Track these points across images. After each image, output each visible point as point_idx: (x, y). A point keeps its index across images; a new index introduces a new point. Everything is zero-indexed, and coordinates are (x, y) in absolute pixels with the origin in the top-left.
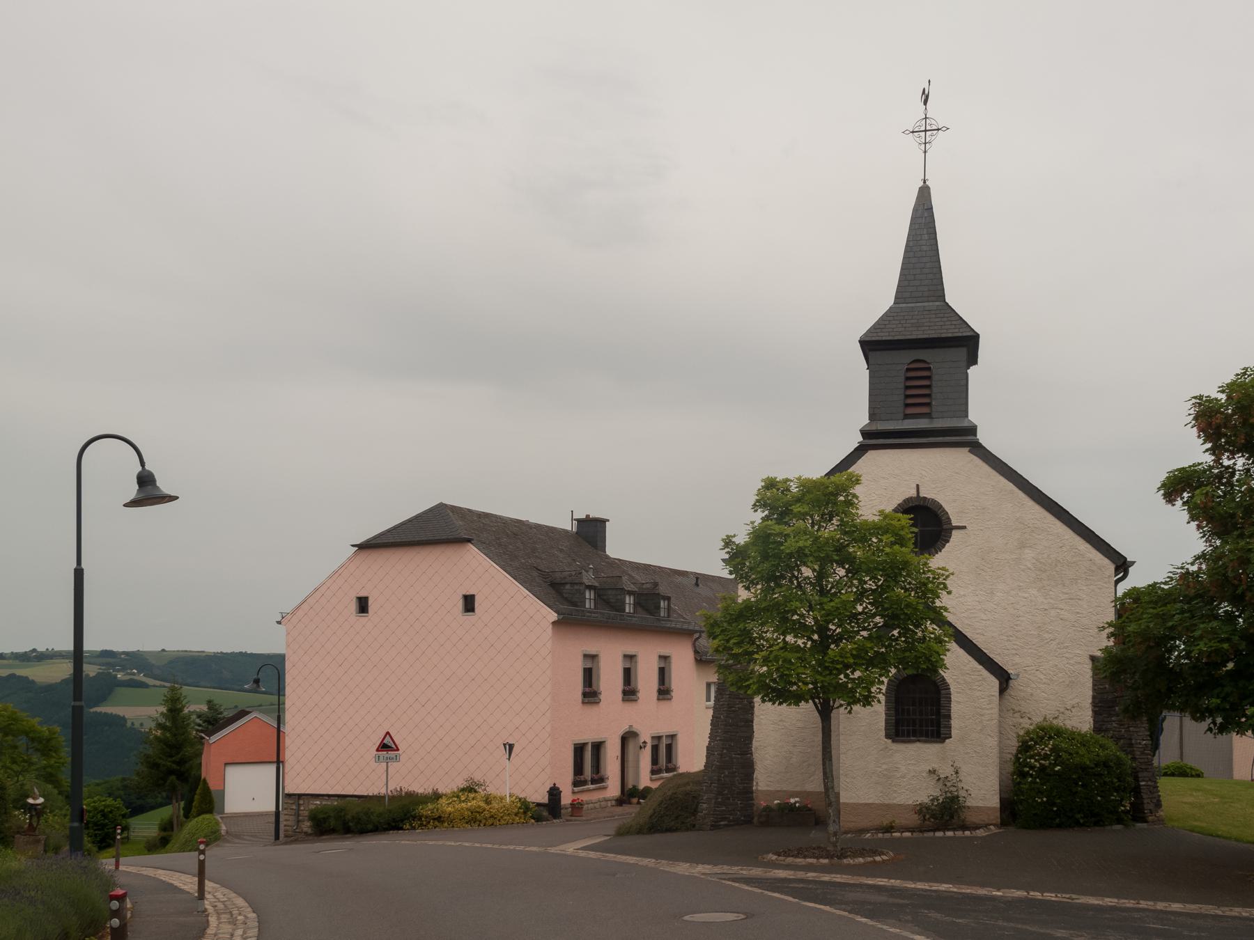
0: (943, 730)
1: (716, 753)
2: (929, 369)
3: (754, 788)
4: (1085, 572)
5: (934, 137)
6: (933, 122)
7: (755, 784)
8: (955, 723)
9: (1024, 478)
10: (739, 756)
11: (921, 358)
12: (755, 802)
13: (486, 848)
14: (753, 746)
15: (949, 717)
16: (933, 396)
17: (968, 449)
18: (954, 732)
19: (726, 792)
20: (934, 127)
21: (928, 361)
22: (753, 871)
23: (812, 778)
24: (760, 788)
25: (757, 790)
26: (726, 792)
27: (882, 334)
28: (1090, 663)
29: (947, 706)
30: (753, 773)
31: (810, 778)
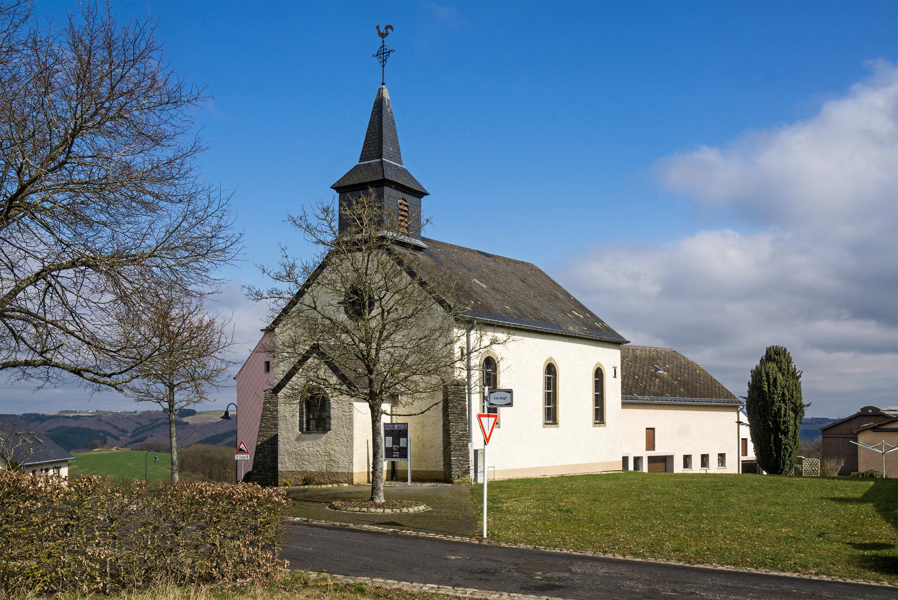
0: (403, 427)
8: (333, 422)
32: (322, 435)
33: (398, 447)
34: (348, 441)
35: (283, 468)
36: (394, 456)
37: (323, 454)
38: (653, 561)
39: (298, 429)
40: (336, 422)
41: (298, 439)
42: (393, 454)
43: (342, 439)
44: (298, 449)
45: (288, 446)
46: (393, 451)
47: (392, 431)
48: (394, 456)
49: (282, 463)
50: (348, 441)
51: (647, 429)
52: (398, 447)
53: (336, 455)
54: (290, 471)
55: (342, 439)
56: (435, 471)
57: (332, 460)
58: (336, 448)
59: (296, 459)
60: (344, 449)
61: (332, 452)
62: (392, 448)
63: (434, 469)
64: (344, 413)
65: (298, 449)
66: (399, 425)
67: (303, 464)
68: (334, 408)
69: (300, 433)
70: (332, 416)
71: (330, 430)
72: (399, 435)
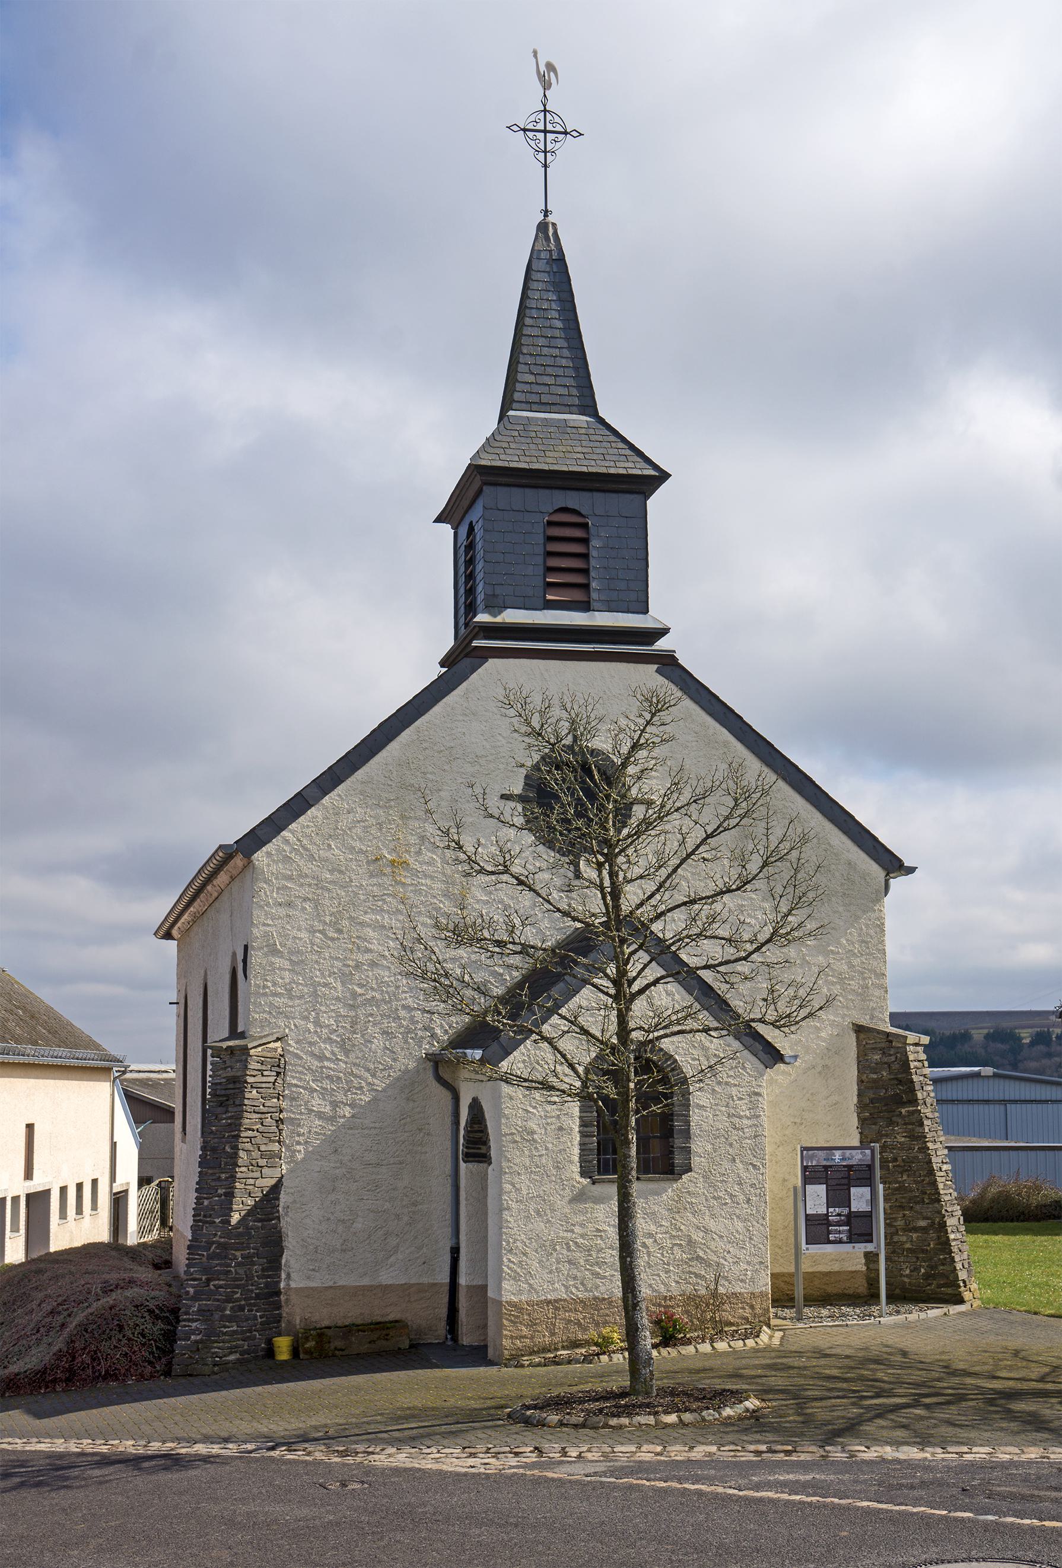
0: (678, 1160)
1: (217, 1221)
2: (585, 526)
3: (282, 1285)
4: (842, 884)
5: (558, 145)
6: (557, 119)
7: (283, 1276)
8: (699, 1146)
9: (745, 722)
10: (259, 1224)
11: (570, 505)
12: (285, 1311)
13: (963, 1519)
14: (281, 1204)
15: (687, 1134)
16: (541, 570)
17: (656, 666)
18: (695, 1161)
19: (238, 1295)
20: (559, 128)
21: (583, 512)
22: (402, 1457)
23: (392, 1259)
24: (293, 1285)
25: (288, 1288)
26: (238, 1295)
27: (586, 463)
28: (853, 1036)
29: (683, 1115)
30: (281, 1256)
31: (388, 1258)
32: (663, 1184)
33: (846, 1211)
34: (748, 1201)
35: (520, 1292)
36: (832, 1237)
37: (668, 1243)
38: (19, 1447)
39: (576, 1168)
40: (709, 1147)
41: (579, 1197)
42: (829, 1233)
43: (731, 1196)
44: (577, 1229)
45: (539, 1225)
46: (829, 1224)
47: (826, 1167)
48: (832, 1237)
49: (516, 1278)
50: (748, 1201)
51: (804, 1149)
52: (846, 1211)
53: (713, 1245)
54: (549, 1302)
55: (731, 1196)
56: (838, 1273)
57: (698, 1258)
58: (712, 1225)
59: (570, 1262)
60: (739, 1225)
61: (697, 1236)
62: (827, 1215)
63: (836, 1267)
64: (736, 1120)
65: (577, 1229)
66: (848, 1152)
67: (597, 1275)
68: (701, 1107)
69: (585, 1181)
70: (694, 1129)
71: (690, 1170)
72: (848, 1177)
